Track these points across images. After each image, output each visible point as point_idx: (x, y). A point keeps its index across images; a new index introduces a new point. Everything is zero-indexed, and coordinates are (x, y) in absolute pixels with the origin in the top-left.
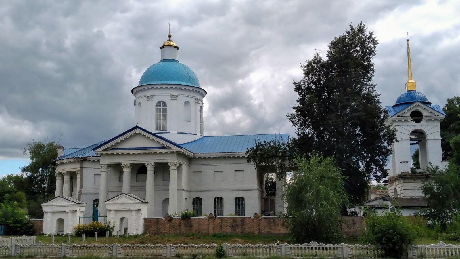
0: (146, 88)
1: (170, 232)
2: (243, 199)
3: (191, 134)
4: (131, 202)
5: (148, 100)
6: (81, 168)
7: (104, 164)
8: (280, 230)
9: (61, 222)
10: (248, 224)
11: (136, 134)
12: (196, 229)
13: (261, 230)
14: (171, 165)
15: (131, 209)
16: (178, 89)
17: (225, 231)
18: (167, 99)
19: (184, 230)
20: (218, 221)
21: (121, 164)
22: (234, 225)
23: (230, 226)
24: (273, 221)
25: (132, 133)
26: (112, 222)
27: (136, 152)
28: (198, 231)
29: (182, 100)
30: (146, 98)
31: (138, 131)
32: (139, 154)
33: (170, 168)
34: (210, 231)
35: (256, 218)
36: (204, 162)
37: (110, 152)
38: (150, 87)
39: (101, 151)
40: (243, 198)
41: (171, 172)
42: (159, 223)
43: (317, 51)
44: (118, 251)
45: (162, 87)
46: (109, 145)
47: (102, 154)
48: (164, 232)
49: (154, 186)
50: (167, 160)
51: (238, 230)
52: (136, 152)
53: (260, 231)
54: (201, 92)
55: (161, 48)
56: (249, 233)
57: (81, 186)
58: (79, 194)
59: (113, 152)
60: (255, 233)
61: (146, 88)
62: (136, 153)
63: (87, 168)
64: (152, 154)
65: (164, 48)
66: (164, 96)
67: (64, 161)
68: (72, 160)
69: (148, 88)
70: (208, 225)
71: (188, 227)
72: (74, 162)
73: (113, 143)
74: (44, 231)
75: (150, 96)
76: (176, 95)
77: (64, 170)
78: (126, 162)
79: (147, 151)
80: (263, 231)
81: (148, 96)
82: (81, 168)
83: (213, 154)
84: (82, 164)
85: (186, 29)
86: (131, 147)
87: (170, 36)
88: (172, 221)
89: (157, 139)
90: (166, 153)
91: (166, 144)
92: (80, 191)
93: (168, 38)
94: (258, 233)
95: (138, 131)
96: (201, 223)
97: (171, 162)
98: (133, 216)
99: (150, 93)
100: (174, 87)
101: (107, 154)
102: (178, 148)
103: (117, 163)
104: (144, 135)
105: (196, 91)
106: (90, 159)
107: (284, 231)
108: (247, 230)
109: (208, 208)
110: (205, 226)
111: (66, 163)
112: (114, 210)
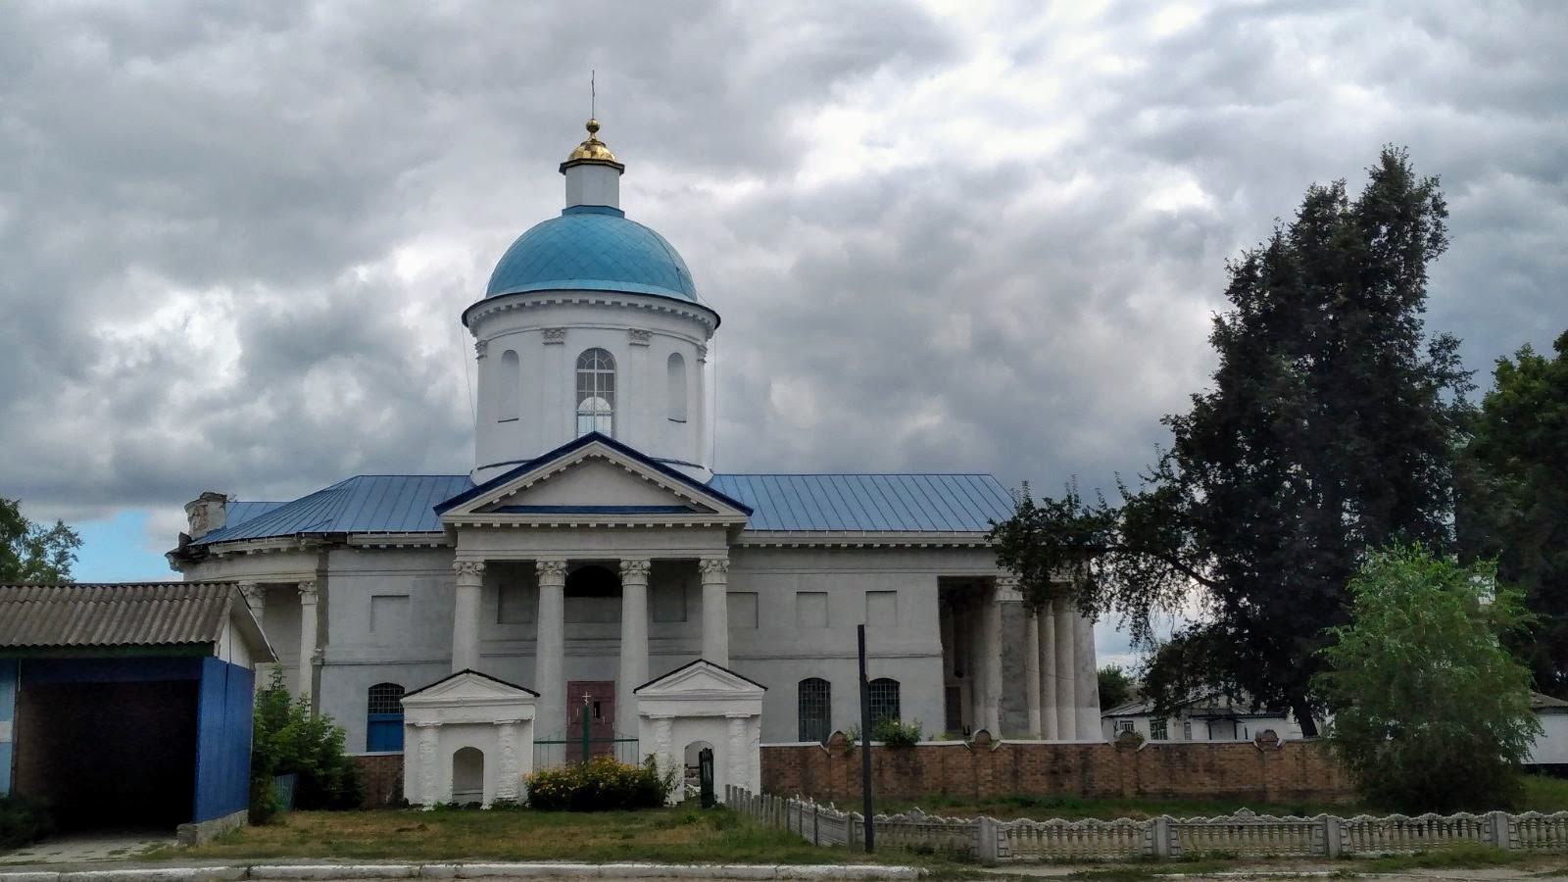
0: (515, 306)
1: (848, 793)
2: (892, 688)
3: (689, 465)
4: (726, 688)
5: (546, 344)
6: (323, 574)
7: (475, 559)
8: (1202, 784)
9: (469, 762)
10: (1102, 764)
11: (588, 459)
12: (935, 782)
13: (1143, 783)
14: (711, 567)
15: (729, 713)
16: (623, 308)
17: (1029, 788)
18: (615, 344)
19: (894, 784)
20: (1006, 755)
21: (534, 562)
22: (1056, 768)
23: (1043, 771)
24: (1178, 754)
25: (577, 456)
26: (662, 760)
27: (593, 520)
28: (940, 789)
29: (662, 347)
30: (540, 338)
31: (597, 449)
32: (602, 527)
33: (542, 582)
34: (981, 788)
35: (1130, 747)
36: (763, 561)
37: (497, 519)
38: (559, 299)
39: (467, 513)
40: (893, 681)
41: (706, 591)
42: (810, 760)
43: (1280, 225)
44: (998, 840)
45: (604, 302)
46: (494, 496)
47: (468, 527)
48: (828, 790)
49: (649, 639)
50: (696, 552)
51: (1072, 784)
52: (593, 520)
53: (1142, 786)
54: (709, 323)
55: (563, 168)
56: (1106, 794)
57: (323, 637)
58: (314, 666)
59: (529, 519)
60: (1126, 793)
61: (515, 306)
62: (574, 525)
63: (344, 573)
64: (629, 528)
65: (580, 167)
66: (590, 329)
67: (249, 548)
68: (284, 545)
69: (498, 309)
70: (974, 768)
71: (906, 774)
72: (293, 551)
73: (510, 488)
74: (409, 794)
75: (558, 330)
76: (646, 332)
77: (245, 578)
78: (552, 555)
79: (631, 520)
80: (1151, 789)
81: (547, 330)
82: (323, 574)
83: (800, 535)
84: (324, 559)
85: (141, 68)
86: (567, 505)
87: (593, 128)
88: (854, 756)
89: (664, 480)
90: (698, 527)
91: (696, 496)
92: (316, 654)
93: (587, 136)
94: (1137, 793)
95: (597, 449)
96: (952, 762)
97: (711, 557)
98: (735, 736)
99: (554, 319)
100: (642, 303)
101: (487, 527)
102: (738, 512)
103: (401, 567)
104: (619, 466)
105: (684, 313)
106: (361, 542)
107: (1215, 785)
108: (1100, 785)
109: (846, 713)
110: (964, 772)
111: (259, 554)
112: (436, 727)
